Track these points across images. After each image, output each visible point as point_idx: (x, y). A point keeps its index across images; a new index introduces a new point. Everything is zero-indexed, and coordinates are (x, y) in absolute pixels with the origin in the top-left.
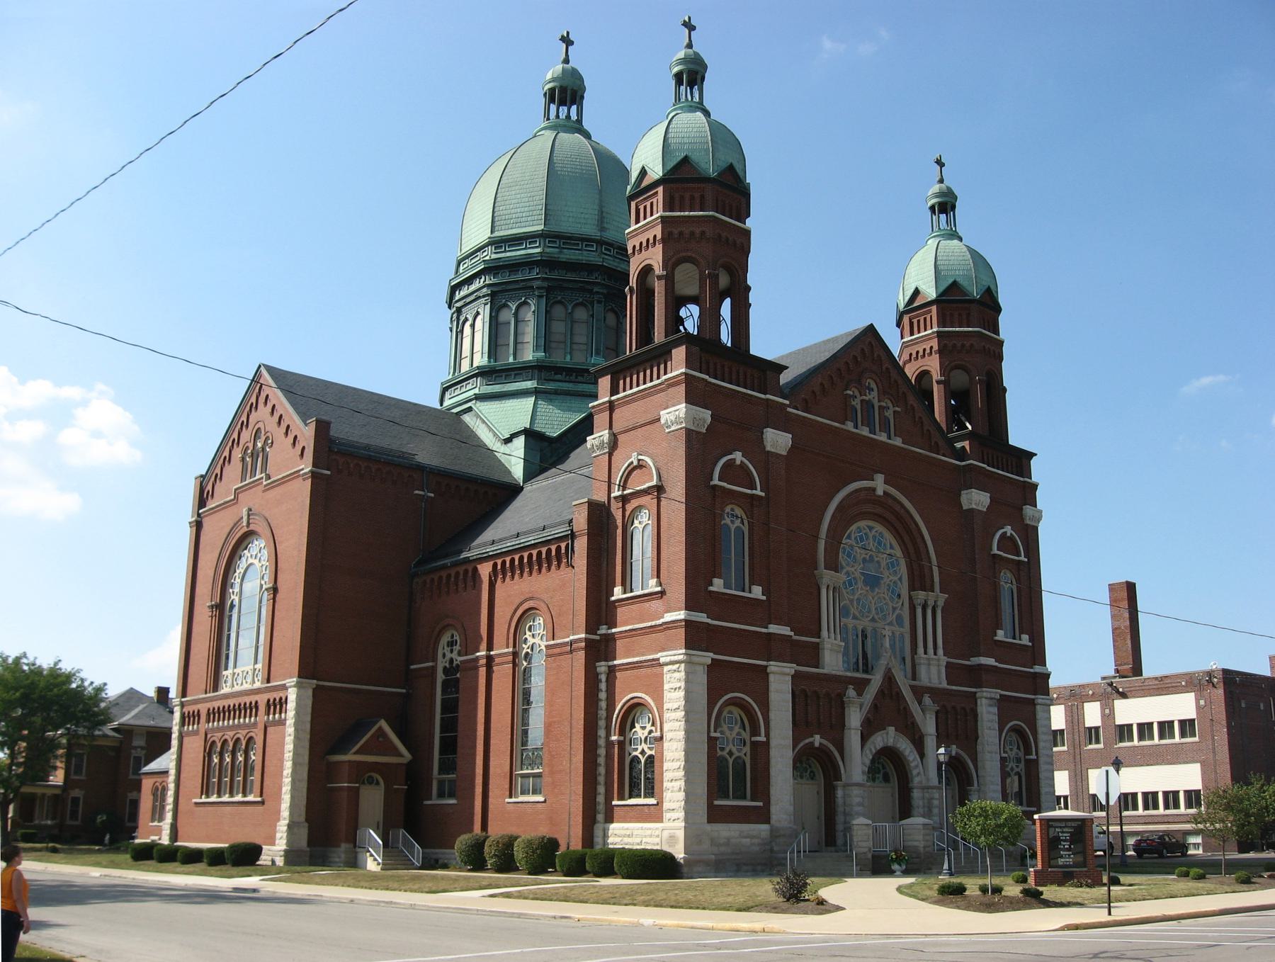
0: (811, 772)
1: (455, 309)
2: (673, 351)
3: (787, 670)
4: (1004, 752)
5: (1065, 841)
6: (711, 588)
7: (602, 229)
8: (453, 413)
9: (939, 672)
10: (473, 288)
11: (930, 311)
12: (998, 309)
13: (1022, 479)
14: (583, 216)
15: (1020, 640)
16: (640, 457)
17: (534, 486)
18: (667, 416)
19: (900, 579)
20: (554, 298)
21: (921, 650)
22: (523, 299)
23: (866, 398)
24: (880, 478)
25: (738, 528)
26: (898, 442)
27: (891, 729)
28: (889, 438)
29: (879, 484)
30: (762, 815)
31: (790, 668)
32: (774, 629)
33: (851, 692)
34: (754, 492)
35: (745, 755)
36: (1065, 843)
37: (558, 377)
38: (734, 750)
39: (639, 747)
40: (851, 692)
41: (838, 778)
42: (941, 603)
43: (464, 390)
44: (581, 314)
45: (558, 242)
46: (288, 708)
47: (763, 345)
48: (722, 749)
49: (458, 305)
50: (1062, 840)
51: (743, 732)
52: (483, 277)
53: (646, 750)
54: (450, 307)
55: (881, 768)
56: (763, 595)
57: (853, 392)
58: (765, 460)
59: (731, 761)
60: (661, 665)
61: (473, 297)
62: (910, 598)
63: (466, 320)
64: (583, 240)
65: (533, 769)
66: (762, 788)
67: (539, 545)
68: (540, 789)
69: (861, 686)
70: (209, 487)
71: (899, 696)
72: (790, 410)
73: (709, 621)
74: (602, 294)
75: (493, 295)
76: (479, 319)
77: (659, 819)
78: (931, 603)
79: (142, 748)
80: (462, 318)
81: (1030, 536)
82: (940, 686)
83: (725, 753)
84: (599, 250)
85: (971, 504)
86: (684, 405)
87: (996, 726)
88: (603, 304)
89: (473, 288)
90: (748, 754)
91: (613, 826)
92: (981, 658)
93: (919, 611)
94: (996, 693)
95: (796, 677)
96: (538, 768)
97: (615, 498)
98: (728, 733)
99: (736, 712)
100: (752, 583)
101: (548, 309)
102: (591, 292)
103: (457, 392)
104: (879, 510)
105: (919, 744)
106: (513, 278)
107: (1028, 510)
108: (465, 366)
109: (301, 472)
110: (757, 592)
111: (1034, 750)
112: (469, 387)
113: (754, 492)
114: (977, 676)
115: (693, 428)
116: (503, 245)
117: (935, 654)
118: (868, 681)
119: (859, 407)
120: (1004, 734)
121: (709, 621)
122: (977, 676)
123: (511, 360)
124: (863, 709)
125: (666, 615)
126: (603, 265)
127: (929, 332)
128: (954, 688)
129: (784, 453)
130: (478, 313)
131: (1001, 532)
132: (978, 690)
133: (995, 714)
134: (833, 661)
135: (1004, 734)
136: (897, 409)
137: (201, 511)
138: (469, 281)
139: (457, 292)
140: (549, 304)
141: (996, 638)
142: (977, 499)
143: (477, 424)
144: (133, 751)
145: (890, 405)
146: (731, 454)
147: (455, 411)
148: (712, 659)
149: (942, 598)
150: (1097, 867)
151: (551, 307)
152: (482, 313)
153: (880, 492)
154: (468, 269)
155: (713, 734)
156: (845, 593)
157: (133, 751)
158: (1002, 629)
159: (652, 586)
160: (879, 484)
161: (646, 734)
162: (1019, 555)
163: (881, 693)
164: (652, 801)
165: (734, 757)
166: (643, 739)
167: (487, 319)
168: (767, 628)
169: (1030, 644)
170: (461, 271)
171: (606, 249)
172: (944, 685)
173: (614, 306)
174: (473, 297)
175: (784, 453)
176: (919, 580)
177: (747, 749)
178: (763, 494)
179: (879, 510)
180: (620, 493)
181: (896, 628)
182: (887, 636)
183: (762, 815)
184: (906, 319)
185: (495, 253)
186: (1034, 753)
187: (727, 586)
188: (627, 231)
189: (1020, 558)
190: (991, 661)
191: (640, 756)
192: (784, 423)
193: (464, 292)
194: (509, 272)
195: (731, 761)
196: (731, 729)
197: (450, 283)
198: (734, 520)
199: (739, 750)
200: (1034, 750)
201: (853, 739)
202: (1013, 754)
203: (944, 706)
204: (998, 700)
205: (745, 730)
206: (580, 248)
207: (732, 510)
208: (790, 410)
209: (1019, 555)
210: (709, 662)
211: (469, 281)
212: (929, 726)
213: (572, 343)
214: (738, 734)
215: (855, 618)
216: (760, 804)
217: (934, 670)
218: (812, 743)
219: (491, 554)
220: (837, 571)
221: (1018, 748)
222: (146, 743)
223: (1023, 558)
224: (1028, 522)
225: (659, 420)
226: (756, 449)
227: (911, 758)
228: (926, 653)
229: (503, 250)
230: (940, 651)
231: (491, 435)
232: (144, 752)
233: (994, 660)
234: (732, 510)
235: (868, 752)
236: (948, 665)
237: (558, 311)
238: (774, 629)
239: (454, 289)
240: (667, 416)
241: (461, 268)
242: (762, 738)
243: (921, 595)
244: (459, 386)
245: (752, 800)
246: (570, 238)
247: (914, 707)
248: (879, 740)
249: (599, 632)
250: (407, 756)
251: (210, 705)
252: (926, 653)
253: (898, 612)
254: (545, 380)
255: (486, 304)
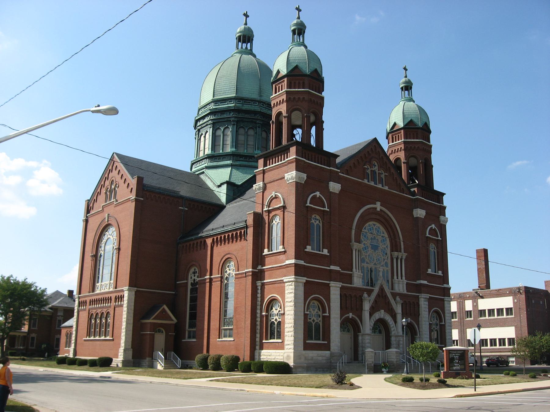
0: (348, 329)
1: (197, 130)
2: (290, 148)
3: (338, 285)
4: (431, 321)
5: (456, 359)
6: (306, 250)
7: (261, 96)
8: (196, 174)
9: (403, 287)
10: (205, 121)
11: (401, 132)
12: (430, 132)
13: (439, 204)
14: (252, 90)
15: (438, 273)
16: (276, 194)
17: (230, 206)
18: (288, 176)
19: (387, 247)
20: (240, 125)
21: (395, 277)
22: (226, 126)
23: (373, 169)
24: (378, 204)
25: (317, 224)
26: (386, 188)
27: (382, 311)
28: (383, 186)
29: (378, 206)
30: (327, 347)
31: (339, 284)
32: (332, 267)
33: (365, 295)
34: (325, 209)
35: (320, 321)
36: (456, 360)
37: (241, 159)
38: (315, 319)
39: (274, 317)
40: (365, 295)
41: (360, 331)
42: (404, 257)
43: (201, 164)
44: (251, 132)
45: (242, 101)
46: (124, 300)
47: (329, 146)
48: (310, 319)
49: (199, 128)
50: (455, 359)
51: (319, 311)
52: (209, 116)
53: (277, 319)
54: (195, 129)
55: (378, 327)
56: (328, 253)
57: (367, 167)
58: (330, 195)
59: (314, 324)
60: (284, 283)
61: (205, 125)
62: (391, 255)
63: (202, 134)
64: (252, 100)
65: (229, 327)
66: (327, 335)
67: (232, 231)
68: (232, 335)
69: (370, 292)
70: (91, 205)
71: (386, 297)
72: (340, 174)
73: (305, 264)
74: (260, 124)
75: (214, 124)
76: (208, 134)
77: (282, 348)
78: (400, 257)
79: (62, 316)
80: (200, 134)
81: (442, 229)
82: (404, 293)
83: (311, 320)
84: (259, 105)
85: (417, 215)
86: (295, 171)
87: (427, 310)
88: (261, 128)
89: (205, 121)
90: (321, 321)
91: (263, 351)
92: (421, 281)
93: (395, 261)
94: (428, 296)
95: (342, 288)
96: (231, 326)
97: (265, 211)
98: (312, 312)
99: (316, 303)
100: (323, 248)
101: (237, 130)
102: (255, 123)
103: (201, 164)
104: (378, 217)
105: (394, 317)
106: (223, 116)
107: (442, 218)
108: (201, 154)
109: (131, 199)
110: (326, 252)
111: (443, 320)
112: (203, 163)
113: (325, 209)
114: (419, 288)
115: (299, 181)
116: (218, 102)
117: (402, 279)
118: (373, 290)
119: (370, 173)
120: (431, 314)
121: (305, 264)
122: (419, 288)
123: (221, 151)
124: (371, 302)
125: (286, 261)
126: (261, 111)
127: (400, 141)
128: (409, 293)
129: (338, 192)
130: (207, 132)
131: (430, 227)
132: (420, 294)
133: (427, 305)
134: (358, 282)
135: (431, 314)
136: (386, 174)
137: (88, 215)
138: (203, 118)
139: (198, 123)
140: (238, 128)
141: (428, 272)
142: (420, 213)
143: (206, 179)
144: (58, 317)
145: (383, 172)
146: (315, 193)
147: (197, 173)
148: (306, 280)
149: (405, 255)
150: (469, 371)
151: (238, 130)
152: (209, 131)
153: (378, 209)
154: (203, 113)
155: (306, 312)
156: (363, 253)
157: (58, 317)
158: (430, 269)
159: (281, 249)
160: (378, 206)
161: (277, 312)
162: (438, 237)
163: (378, 295)
164: (280, 341)
165: (315, 322)
166: (276, 314)
167: (211, 134)
168: (329, 267)
169: (442, 275)
170: (200, 114)
171: (262, 105)
172: (405, 292)
173: (265, 129)
174: (205, 125)
175: (338, 192)
176: (395, 247)
177: (321, 319)
178: (328, 210)
179: (378, 217)
180: (267, 209)
181: (385, 268)
182: (381, 271)
183: (327, 347)
184: (390, 136)
185: (215, 106)
186: (443, 322)
187: (312, 249)
188: (271, 97)
189: (438, 238)
190: (425, 282)
191: (275, 321)
192: (338, 179)
193: (201, 122)
194: (221, 114)
195: (314, 324)
196: (314, 310)
197: (195, 119)
198: (316, 221)
199: (436, 327)
200: (443, 320)
201: (366, 315)
202: (434, 322)
203: (405, 301)
204: (428, 299)
205: (320, 311)
206: (251, 104)
207: (315, 216)
208: (340, 174)
209: (438, 237)
210: (305, 281)
211: (203, 118)
212: (398, 310)
213: (247, 145)
214: (317, 312)
215: (367, 263)
216: (326, 342)
217: (401, 285)
218: (349, 317)
219: (212, 234)
220: (360, 243)
221: (437, 319)
222: (63, 314)
223: (439, 238)
224: (442, 223)
225: (284, 178)
226: (325, 190)
227: (391, 323)
228: (397, 278)
229: (218, 104)
230: (404, 278)
231: (212, 184)
232: (62, 318)
233: (427, 282)
234: (315, 216)
235: (372, 321)
236: (407, 284)
237: (242, 131)
238: (332, 267)
239: (197, 121)
240: (288, 176)
241: (200, 112)
242: (327, 314)
243: (396, 254)
244: (199, 163)
245: (323, 341)
246: (246, 100)
247: (392, 301)
248: (378, 315)
249: (258, 268)
250: (175, 320)
251: (91, 298)
252: (397, 278)
253: (386, 260)
254: (236, 160)
255: (210, 128)
